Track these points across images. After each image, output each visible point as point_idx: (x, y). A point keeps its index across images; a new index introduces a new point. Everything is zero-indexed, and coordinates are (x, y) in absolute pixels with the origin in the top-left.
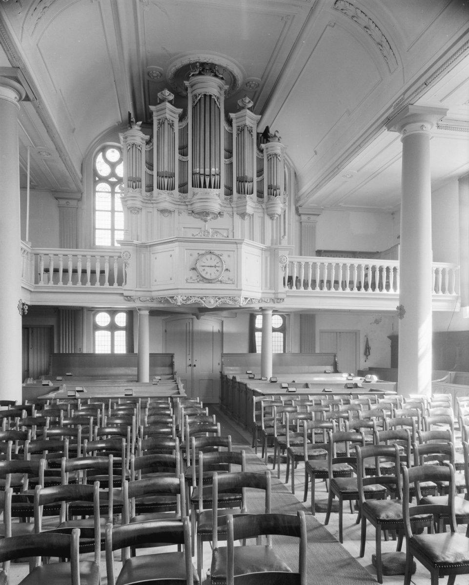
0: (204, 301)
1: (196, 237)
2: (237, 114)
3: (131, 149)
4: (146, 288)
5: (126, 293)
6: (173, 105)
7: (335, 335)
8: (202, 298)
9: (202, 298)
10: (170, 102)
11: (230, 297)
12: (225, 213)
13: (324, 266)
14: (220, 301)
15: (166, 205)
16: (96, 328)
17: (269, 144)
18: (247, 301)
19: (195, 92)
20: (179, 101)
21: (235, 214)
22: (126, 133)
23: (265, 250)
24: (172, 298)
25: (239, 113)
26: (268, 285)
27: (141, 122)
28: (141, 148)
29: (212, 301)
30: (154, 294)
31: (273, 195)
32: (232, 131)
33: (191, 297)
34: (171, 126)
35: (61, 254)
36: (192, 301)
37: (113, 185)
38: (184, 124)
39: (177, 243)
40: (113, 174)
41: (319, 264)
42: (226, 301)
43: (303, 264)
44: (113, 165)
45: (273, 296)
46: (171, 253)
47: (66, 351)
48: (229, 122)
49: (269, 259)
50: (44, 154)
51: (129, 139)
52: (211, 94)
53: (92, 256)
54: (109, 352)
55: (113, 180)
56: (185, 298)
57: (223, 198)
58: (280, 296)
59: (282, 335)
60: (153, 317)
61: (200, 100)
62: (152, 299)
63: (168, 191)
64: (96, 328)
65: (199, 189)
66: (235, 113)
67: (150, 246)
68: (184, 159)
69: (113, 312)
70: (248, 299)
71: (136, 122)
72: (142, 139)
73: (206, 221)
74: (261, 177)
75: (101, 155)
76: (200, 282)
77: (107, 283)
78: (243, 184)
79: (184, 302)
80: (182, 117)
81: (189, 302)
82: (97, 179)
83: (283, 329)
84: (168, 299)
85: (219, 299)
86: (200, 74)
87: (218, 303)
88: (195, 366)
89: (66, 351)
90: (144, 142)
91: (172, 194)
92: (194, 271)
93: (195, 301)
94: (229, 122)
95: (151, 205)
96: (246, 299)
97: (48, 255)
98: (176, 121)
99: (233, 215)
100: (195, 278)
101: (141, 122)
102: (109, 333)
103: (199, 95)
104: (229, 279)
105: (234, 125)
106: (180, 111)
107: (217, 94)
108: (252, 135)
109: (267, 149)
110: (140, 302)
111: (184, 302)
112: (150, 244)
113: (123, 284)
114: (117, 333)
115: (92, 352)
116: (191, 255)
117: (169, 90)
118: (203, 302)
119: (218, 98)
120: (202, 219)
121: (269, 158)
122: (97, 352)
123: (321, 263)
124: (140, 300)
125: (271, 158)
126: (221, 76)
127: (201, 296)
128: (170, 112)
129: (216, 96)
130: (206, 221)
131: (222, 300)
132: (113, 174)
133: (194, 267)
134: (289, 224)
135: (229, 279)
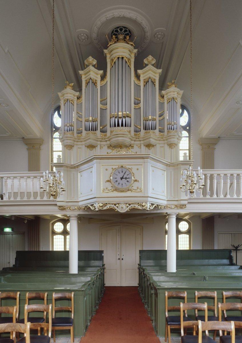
0: (117, 207)
1: (110, 154)
3: (66, 103)
4: (75, 200)
5: (59, 204)
6: (95, 68)
7: (231, 236)
9: (115, 205)
10: (94, 66)
11: (138, 203)
12: (135, 146)
13: (221, 177)
15: (91, 142)
16: (54, 233)
18: (154, 206)
19: (112, 56)
20: (102, 65)
21: (142, 146)
22: (63, 91)
24: (92, 205)
27: (73, 84)
28: (74, 103)
30: (80, 204)
31: (172, 129)
33: (106, 204)
34: (94, 84)
36: (108, 207)
38: (104, 83)
39: (95, 161)
41: (215, 175)
42: (135, 207)
46: (90, 170)
47: (36, 249)
48: (138, 77)
49: (172, 173)
50: (4, 105)
51: (66, 95)
52: (123, 56)
54: (63, 250)
56: (101, 205)
59: (188, 236)
60: (214, 297)
61: (115, 62)
62: (79, 209)
63: (93, 132)
64: (54, 233)
65: (114, 128)
66: (142, 69)
67: (78, 166)
68: (103, 107)
70: (155, 205)
71: (69, 84)
72: (74, 95)
74: (163, 116)
78: (148, 122)
79: (101, 208)
80: (103, 77)
81: (105, 208)
83: (188, 232)
84: (89, 207)
85: (130, 205)
86: (115, 42)
88: (122, 259)
89: (36, 249)
90: (76, 98)
91: (95, 133)
93: (110, 207)
94: (138, 77)
95: (81, 143)
96: (152, 204)
98: (99, 79)
100: (110, 188)
101: (73, 84)
102: (63, 237)
103: (115, 58)
105: (142, 78)
106: (101, 72)
107: (128, 56)
108: (155, 85)
112: (76, 165)
113: (58, 197)
115: (51, 250)
116: (106, 170)
117: (92, 57)
118: (116, 208)
119: (129, 59)
121: (168, 101)
122: (55, 250)
125: (170, 101)
127: (115, 203)
128: (94, 74)
129: (127, 58)
131: (132, 205)
133: (109, 179)
135: (138, 188)
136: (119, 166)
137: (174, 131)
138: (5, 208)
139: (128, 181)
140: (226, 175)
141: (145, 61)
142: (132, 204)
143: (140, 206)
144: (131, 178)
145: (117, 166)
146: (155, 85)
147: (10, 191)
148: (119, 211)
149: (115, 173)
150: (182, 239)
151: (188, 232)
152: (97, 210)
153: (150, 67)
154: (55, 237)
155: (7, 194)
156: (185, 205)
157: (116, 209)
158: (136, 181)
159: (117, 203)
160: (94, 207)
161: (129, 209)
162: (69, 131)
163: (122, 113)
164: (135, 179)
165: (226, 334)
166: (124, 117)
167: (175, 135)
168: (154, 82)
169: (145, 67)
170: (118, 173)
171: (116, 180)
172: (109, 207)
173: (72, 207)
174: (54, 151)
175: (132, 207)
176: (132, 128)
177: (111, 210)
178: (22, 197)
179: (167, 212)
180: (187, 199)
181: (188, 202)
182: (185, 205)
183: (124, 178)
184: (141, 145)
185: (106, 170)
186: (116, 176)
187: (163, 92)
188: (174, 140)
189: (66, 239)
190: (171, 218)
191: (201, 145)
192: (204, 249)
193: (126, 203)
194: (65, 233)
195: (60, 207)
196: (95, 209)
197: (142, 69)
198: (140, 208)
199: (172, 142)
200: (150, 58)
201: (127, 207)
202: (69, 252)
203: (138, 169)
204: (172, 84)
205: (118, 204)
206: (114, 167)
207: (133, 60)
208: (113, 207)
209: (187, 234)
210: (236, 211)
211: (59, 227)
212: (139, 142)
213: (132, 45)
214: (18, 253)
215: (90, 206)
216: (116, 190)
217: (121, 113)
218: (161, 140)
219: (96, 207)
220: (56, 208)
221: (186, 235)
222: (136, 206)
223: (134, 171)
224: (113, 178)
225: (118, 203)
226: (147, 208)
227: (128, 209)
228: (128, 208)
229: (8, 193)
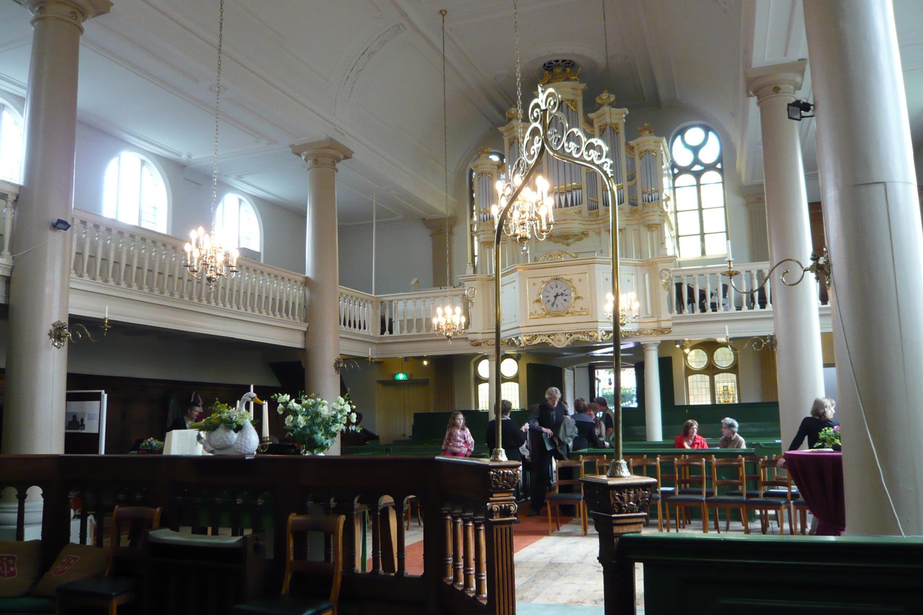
2: (597, 113)
5: (470, 337)
8: (549, 336)
9: (549, 336)
12: (590, 233)
14: (571, 338)
16: (479, 380)
17: (639, 140)
23: (642, 266)
25: (599, 111)
26: (649, 312)
29: (563, 338)
32: (594, 132)
33: (536, 335)
35: (684, 275)
37: (698, 175)
40: (696, 161)
43: (755, 273)
44: (696, 150)
45: (655, 326)
49: (647, 276)
53: (699, 275)
55: (697, 168)
57: (587, 215)
58: (664, 325)
59: (734, 376)
64: (479, 380)
69: (710, 346)
73: (568, 245)
74: (633, 181)
75: (679, 138)
76: (547, 316)
77: (757, 306)
81: (535, 342)
82: (719, 166)
83: (733, 369)
85: (571, 335)
87: (569, 340)
89: (685, 476)
92: (538, 303)
93: (541, 340)
97: (692, 276)
99: (600, 233)
100: (540, 312)
102: (707, 378)
104: (581, 309)
109: (638, 145)
110: (488, 346)
111: (527, 343)
114: (706, 382)
118: (550, 341)
120: (563, 243)
123: (746, 272)
124: (488, 344)
126: (574, 78)
129: (568, 100)
130: (568, 245)
131: (574, 336)
132: (696, 161)
134: (504, 257)
135: (581, 309)
136: (553, 277)
137: (651, 204)
138: (396, 347)
139: (565, 300)
140: (750, 271)
141: (598, 101)
142: (574, 334)
143: (587, 336)
144: (570, 295)
145: (550, 278)
146: (617, 133)
147: (402, 318)
148: (556, 346)
149: (546, 290)
150: (695, 384)
151: (733, 369)
152: (522, 345)
153: (606, 109)
154: (690, 378)
155: (399, 322)
156: (670, 329)
157: (550, 344)
158: (578, 298)
159: (552, 334)
160: (520, 341)
161: (570, 342)
162: (487, 220)
163: (565, 186)
164: (577, 296)
165: (688, 521)
166: (568, 191)
167: (655, 212)
168: (615, 129)
169: (598, 109)
170: (549, 289)
171: (548, 299)
172: (539, 340)
173: (490, 340)
174: (698, 235)
175: (574, 339)
176: (585, 206)
177: (544, 344)
178: (419, 330)
179: (640, 341)
180: (671, 319)
181: (674, 324)
182: (670, 329)
183: (559, 295)
184: (600, 231)
185: (534, 284)
186: (547, 294)
187: (632, 143)
188: (655, 219)
189: (478, 390)
190: (648, 350)
191: (744, 197)
192: (744, 401)
193: (566, 334)
194: (711, 370)
195: (472, 341)
196: (520, 344)
197: (594, 111)
198: (586, 339)
199: (652, 222)
200: (605, 96)
201: (568, 339)
202: (489, 414)
203: (580, 280)
204: (645, 129)
205: (554, 335)
206: (546, 279)
207: (580, 100)
208: (546, 340)
209: (732, 373)
210: (739, 334)
211: (484, 369)
212: (597, 226)
213: (575, 80)
214: (417, 416)
215: (514, 339)
216: (549, 314)
217: (563, 186)
218: (633, 220)
219: (522, 342)
220: (468, 343)
221: (729, 374)
222: (580, 337)
223: (575, 283)
224: (543, 297)
225: (554, 334)
226: (597, 339)
227: (568, 342)
228: (569, 340)
229: (400, 321)
